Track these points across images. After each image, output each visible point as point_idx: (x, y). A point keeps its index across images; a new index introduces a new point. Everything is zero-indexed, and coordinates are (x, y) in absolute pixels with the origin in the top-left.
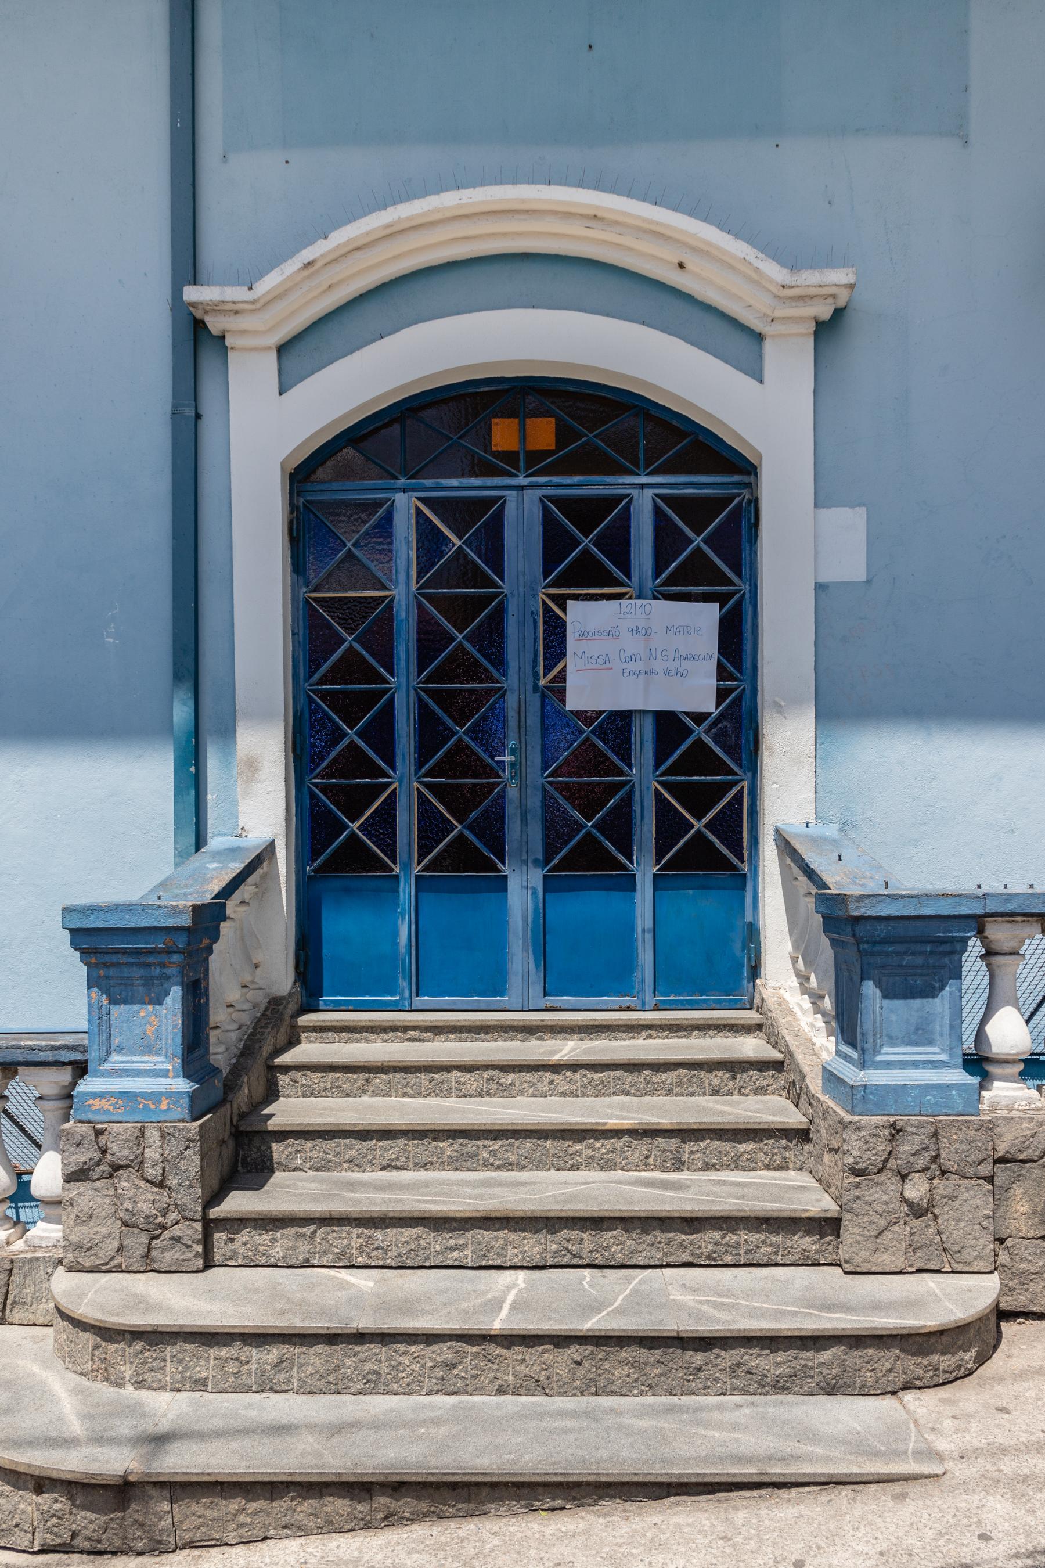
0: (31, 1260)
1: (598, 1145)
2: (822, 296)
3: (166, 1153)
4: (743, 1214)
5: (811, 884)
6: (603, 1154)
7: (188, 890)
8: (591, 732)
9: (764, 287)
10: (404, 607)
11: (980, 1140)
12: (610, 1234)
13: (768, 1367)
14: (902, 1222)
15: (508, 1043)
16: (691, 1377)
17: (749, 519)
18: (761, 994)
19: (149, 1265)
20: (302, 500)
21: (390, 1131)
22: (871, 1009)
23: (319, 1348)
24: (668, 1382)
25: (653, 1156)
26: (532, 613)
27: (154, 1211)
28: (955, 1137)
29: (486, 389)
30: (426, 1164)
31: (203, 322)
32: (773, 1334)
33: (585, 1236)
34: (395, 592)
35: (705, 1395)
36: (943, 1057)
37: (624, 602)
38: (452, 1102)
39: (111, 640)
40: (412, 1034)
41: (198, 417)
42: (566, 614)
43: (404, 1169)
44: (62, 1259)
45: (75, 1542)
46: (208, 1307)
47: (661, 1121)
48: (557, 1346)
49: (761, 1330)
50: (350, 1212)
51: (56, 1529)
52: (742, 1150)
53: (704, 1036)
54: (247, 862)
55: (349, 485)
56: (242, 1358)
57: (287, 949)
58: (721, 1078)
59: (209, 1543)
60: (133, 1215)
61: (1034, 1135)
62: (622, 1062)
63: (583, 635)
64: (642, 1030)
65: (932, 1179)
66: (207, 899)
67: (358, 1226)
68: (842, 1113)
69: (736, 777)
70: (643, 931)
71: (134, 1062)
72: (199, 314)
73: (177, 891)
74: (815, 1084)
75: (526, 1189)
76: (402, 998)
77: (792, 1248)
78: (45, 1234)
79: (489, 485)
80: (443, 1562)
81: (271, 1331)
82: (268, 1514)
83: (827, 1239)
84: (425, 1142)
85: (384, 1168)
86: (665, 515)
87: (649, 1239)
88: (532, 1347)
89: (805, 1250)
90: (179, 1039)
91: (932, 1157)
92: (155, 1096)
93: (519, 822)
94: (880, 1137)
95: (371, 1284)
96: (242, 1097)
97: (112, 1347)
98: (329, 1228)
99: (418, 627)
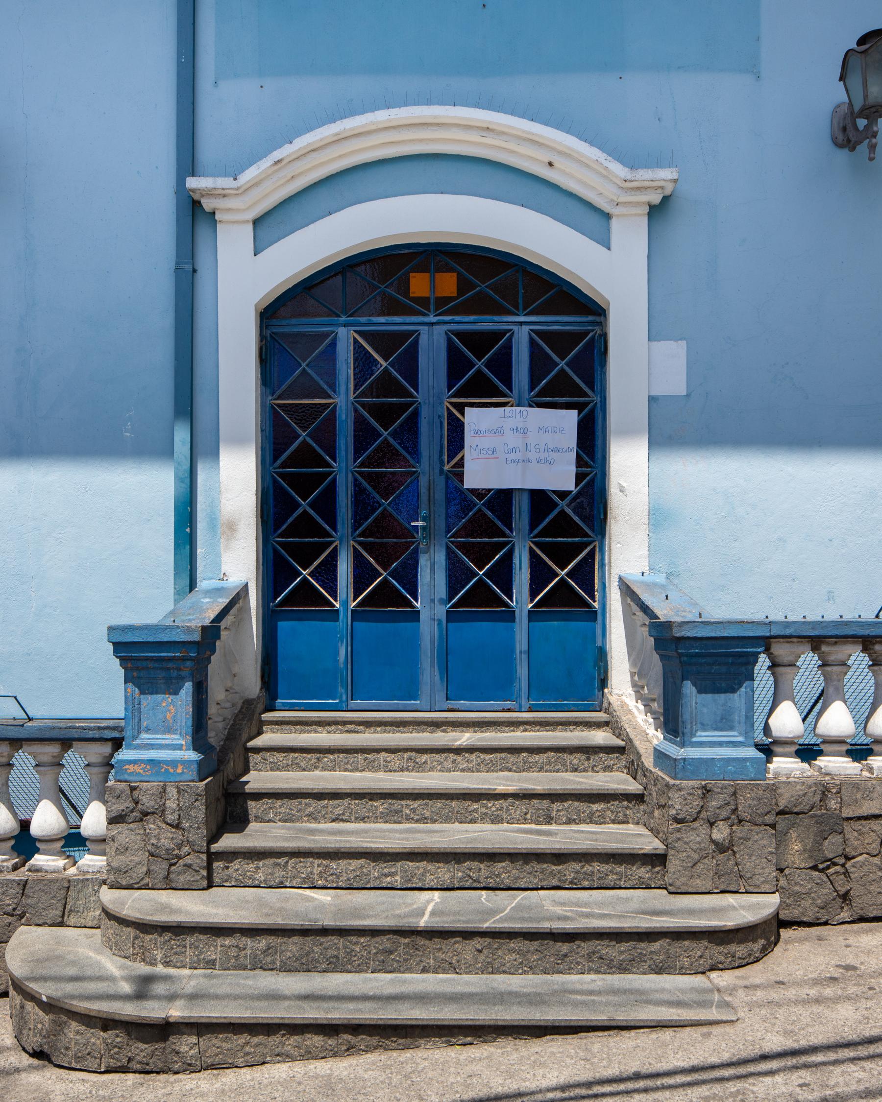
0: (83, 881)
1: (490, 805)
2: (653, 187)
3: (181, 804)
4: (596, 851)
5: (646, 617)
6: (494, 811)
7: (191, 617)
8: (483, 504)
9: (611, 180)
10: (344, 412)
11: (766, 798)
12: (500, 865)
13: (614, 955)
14: (710, 856)
15: (421, 735)
16: (560, 961)
17: (600, 348)
18: (608, 699)
19: (169, 885)
20: (269, 332)
21: (338, 794)
22: (689, 704)
23: (295, 939)
24: (543, 965)
25: (530, 813)
26: (439, 416)
27: (172, 846)
28: (748, 795)
29: (406, 252)
30: (364, 818)
31: (199, 202)
32: (619, 931)
33: (482, 866)
34: (337, 400)
35: (569, 974)
36: (741, 739)
37: (507, 409)
38: (381, 775)
39: (128, 434)
40: (349, 727)
41: (194, 271)
42: (464, 417)
43: (348, 821)
44: (106, 880)
45: (130, 1065)
46: (215, 911)
47: (536, 787)
48: (465, 938)
49: (610, 928)
50: (313, 848)
51: (117, 1056)
52: (595, 809)
53: (566, 730)
54: (231, 598)
55: (304, 320)
56: (241, 946)
57: (256, 664)
58: (579, 759)
59: (224, 1066)
60: (158, 848)
61: (805, 795)
62: (506, 747)
63: (477, 433)
64: (520, 725)
65: (732, 826)
66: (207, 623)
67: (319, 858)
68: (667, 779)
69: (590, 539)
70: (521, 652)
71: (157, 739)
72: (196, 197)
73: (183, 618)
74: (648, 761)
75: (439, 835)
76: (341, 701)
77: (631, 876)
78: (92, 863)
79: (407, 321)
80: (390, 1075)
81: (261, 927)
82: (266, 1046)
83: (657, 869)
84: (363, 801)
85: (333, 821)
86: (538, 345)
87: (528, 868)
88: (447, 939)
89: (640, 877)
90: (190, 723)
91: (732, 810)
92: (174, 763)
93: (428, 571)
94: (695, 795)
95: (329, 899)
96: (230, 769)
97: (148, 937)
98: (297, 860)
99: (355, 426)
